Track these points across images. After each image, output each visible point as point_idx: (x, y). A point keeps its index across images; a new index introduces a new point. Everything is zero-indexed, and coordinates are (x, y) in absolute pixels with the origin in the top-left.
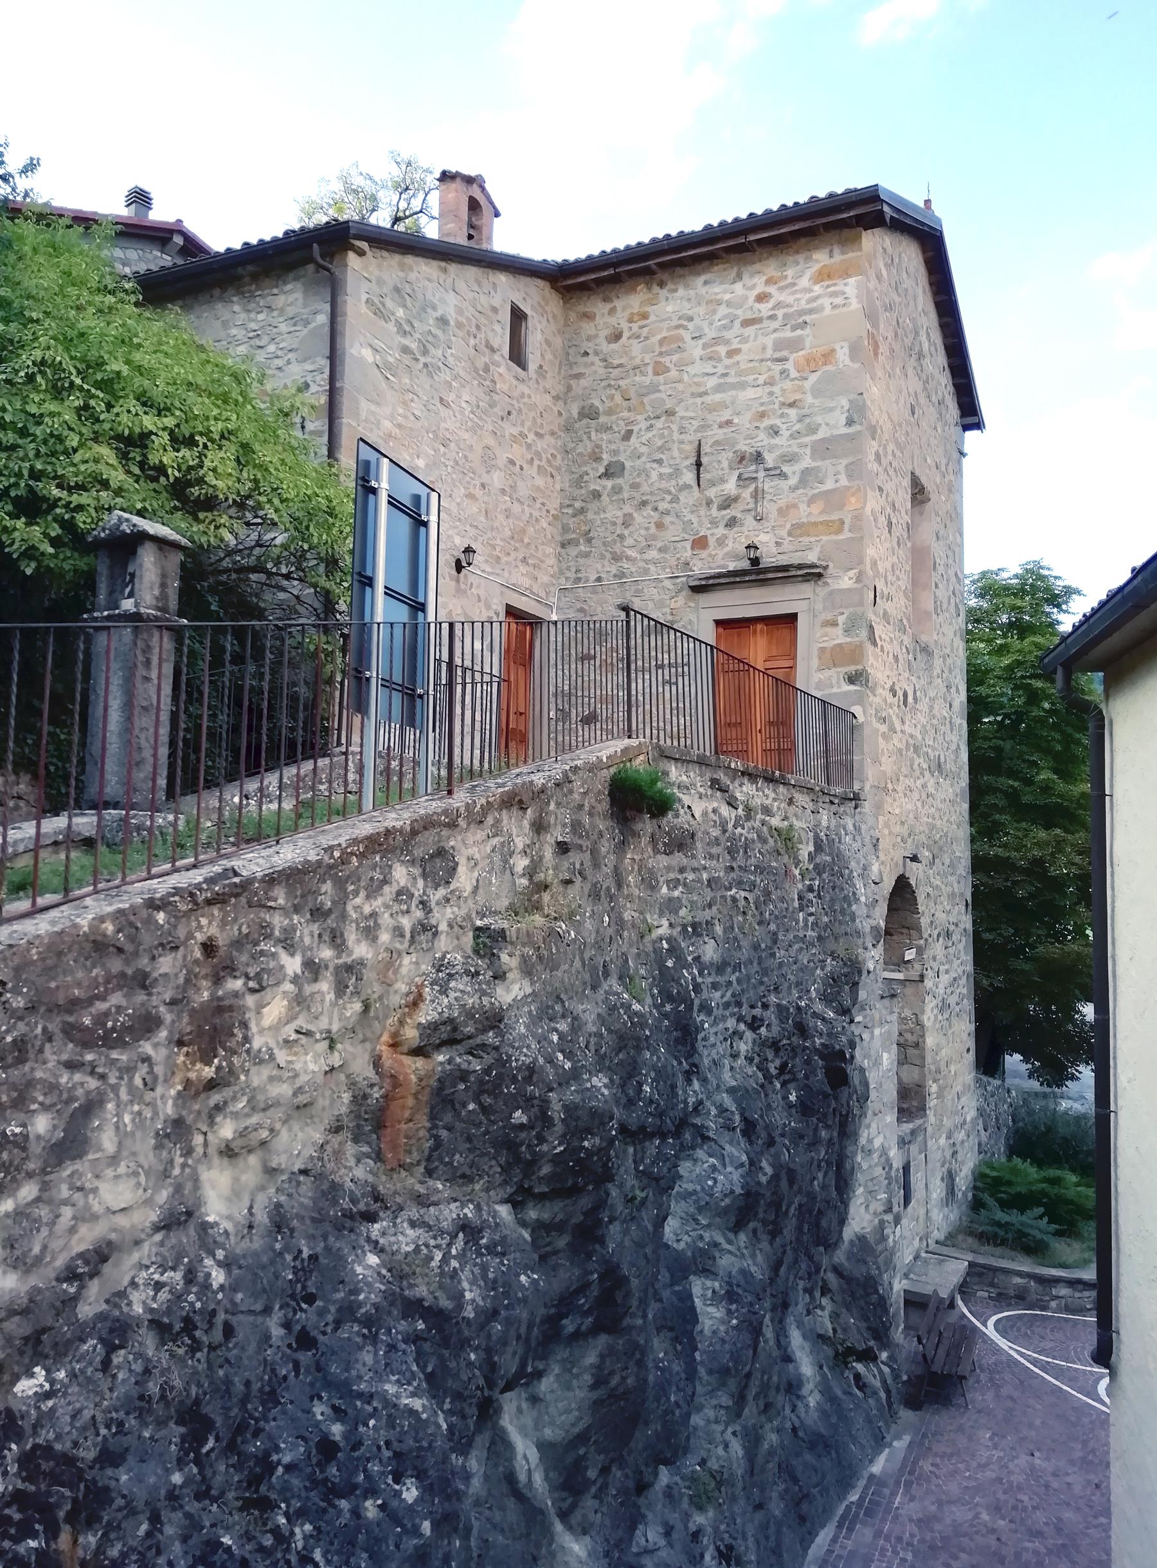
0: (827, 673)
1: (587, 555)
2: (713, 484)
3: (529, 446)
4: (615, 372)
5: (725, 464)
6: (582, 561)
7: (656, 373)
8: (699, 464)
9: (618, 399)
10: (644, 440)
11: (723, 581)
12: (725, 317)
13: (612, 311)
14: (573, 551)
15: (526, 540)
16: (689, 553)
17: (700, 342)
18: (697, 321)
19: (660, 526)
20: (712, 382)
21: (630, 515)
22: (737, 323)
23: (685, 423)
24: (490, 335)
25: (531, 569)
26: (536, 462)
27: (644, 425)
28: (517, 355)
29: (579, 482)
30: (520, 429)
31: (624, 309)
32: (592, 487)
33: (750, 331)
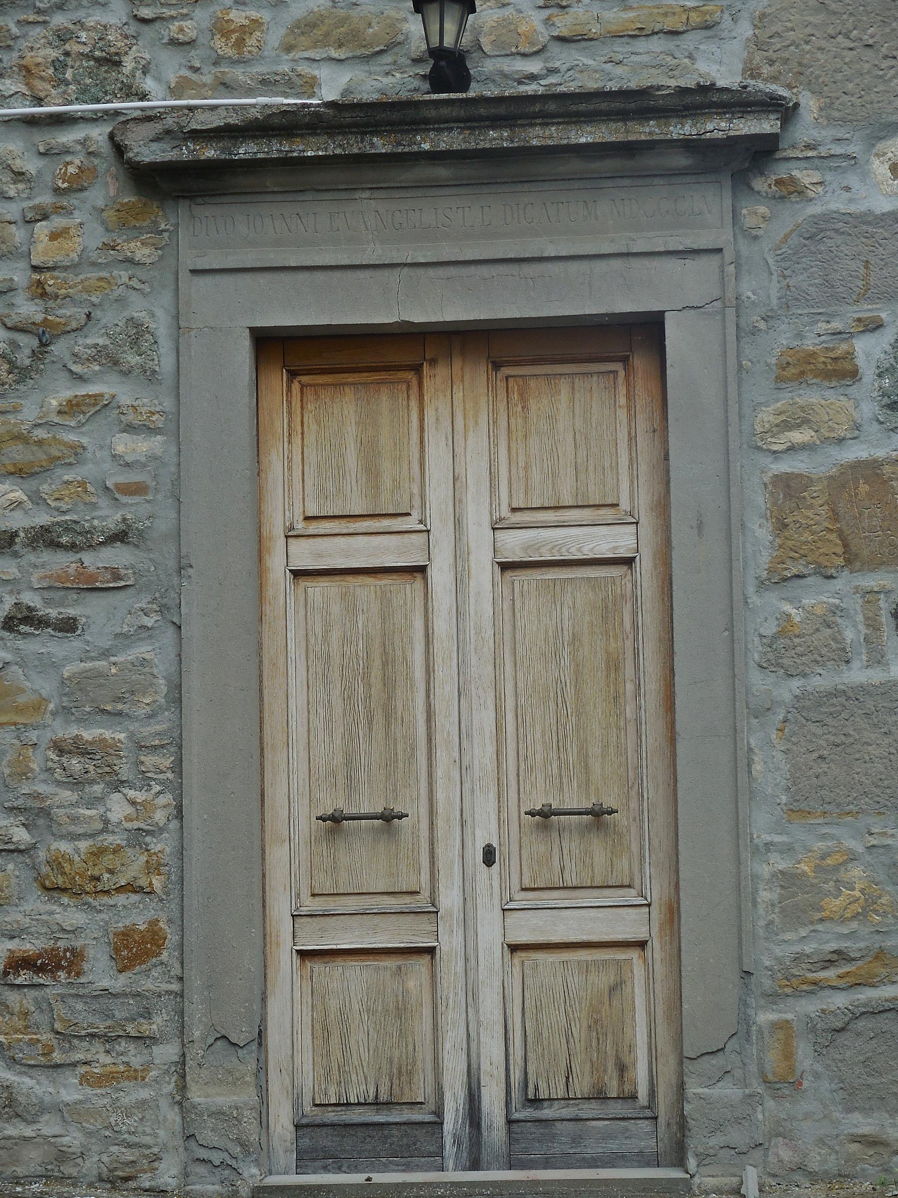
0: (816, 597)
11: (310, 148)
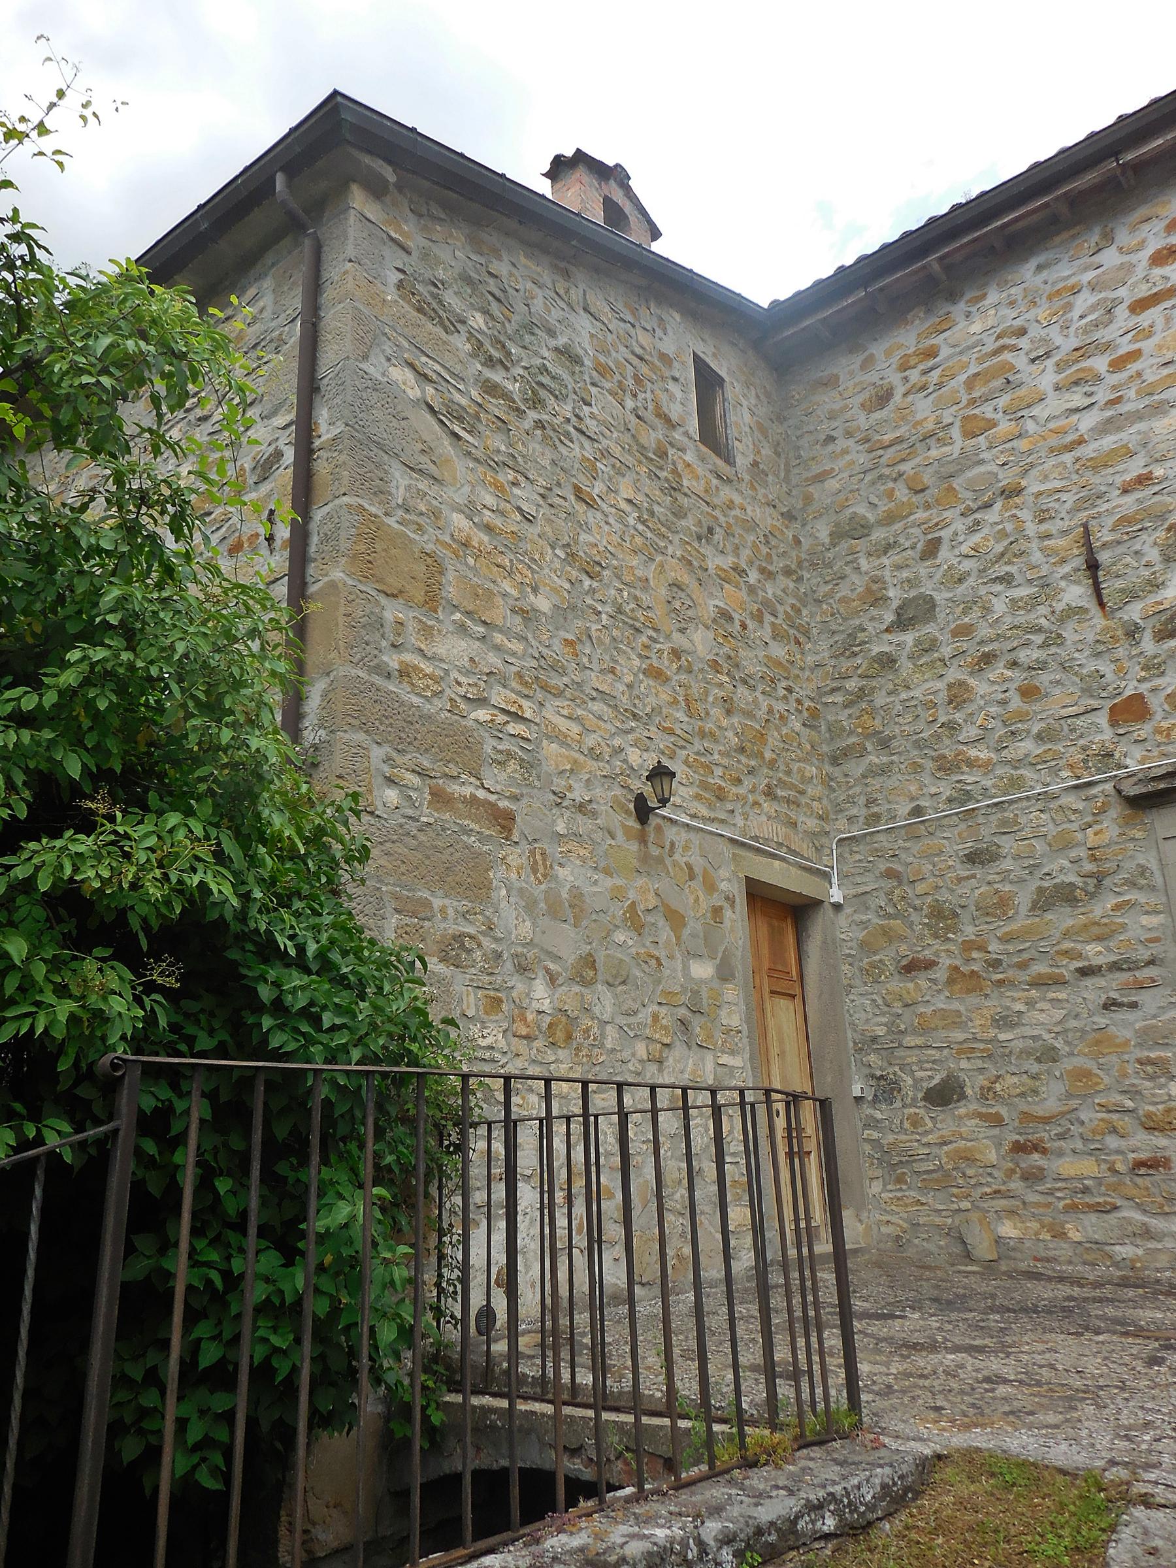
1: (884, 771)
2: (1133, 596)
3: (752, 590)
4: (890, 454)
5: (1153, 555)
6: (875, 783)
7: (969, 434)
8: (1093, 566)
9: (902, 493)
10: (965, 549)
12: (1093, 308)
13: (868, 364)
14: (856, 768)
15: (768, 755)
16: (1107, 734)
17: (1050, 363)
18: (1035, 331)
19: (1029, 692)
20: (1087, 422)
21: (962, 684)
22: (1122, 312)
23: (1047, 502)
24: (663, 397)
25: (784, 808)
26: (768, 618)
27: (960, 525)
28: (711, 435)
29: (850, 646)
30: (730, 560)
31: (888, 354)
32: (876, 650)
33: (1154, 315)
